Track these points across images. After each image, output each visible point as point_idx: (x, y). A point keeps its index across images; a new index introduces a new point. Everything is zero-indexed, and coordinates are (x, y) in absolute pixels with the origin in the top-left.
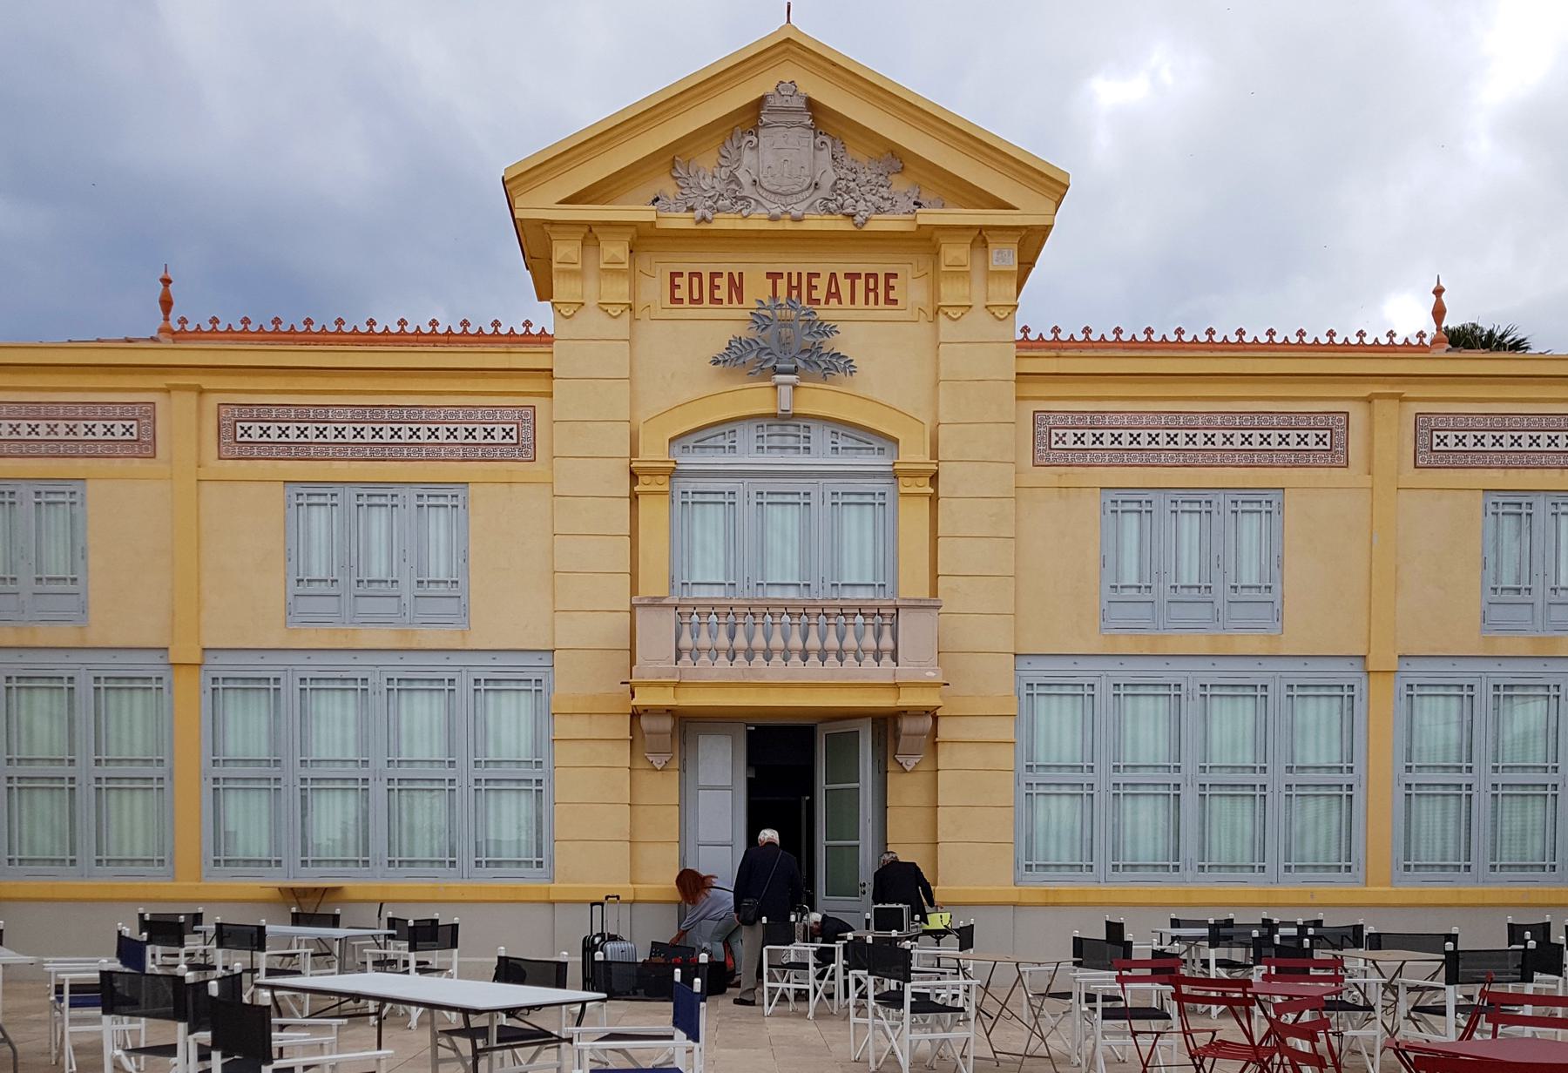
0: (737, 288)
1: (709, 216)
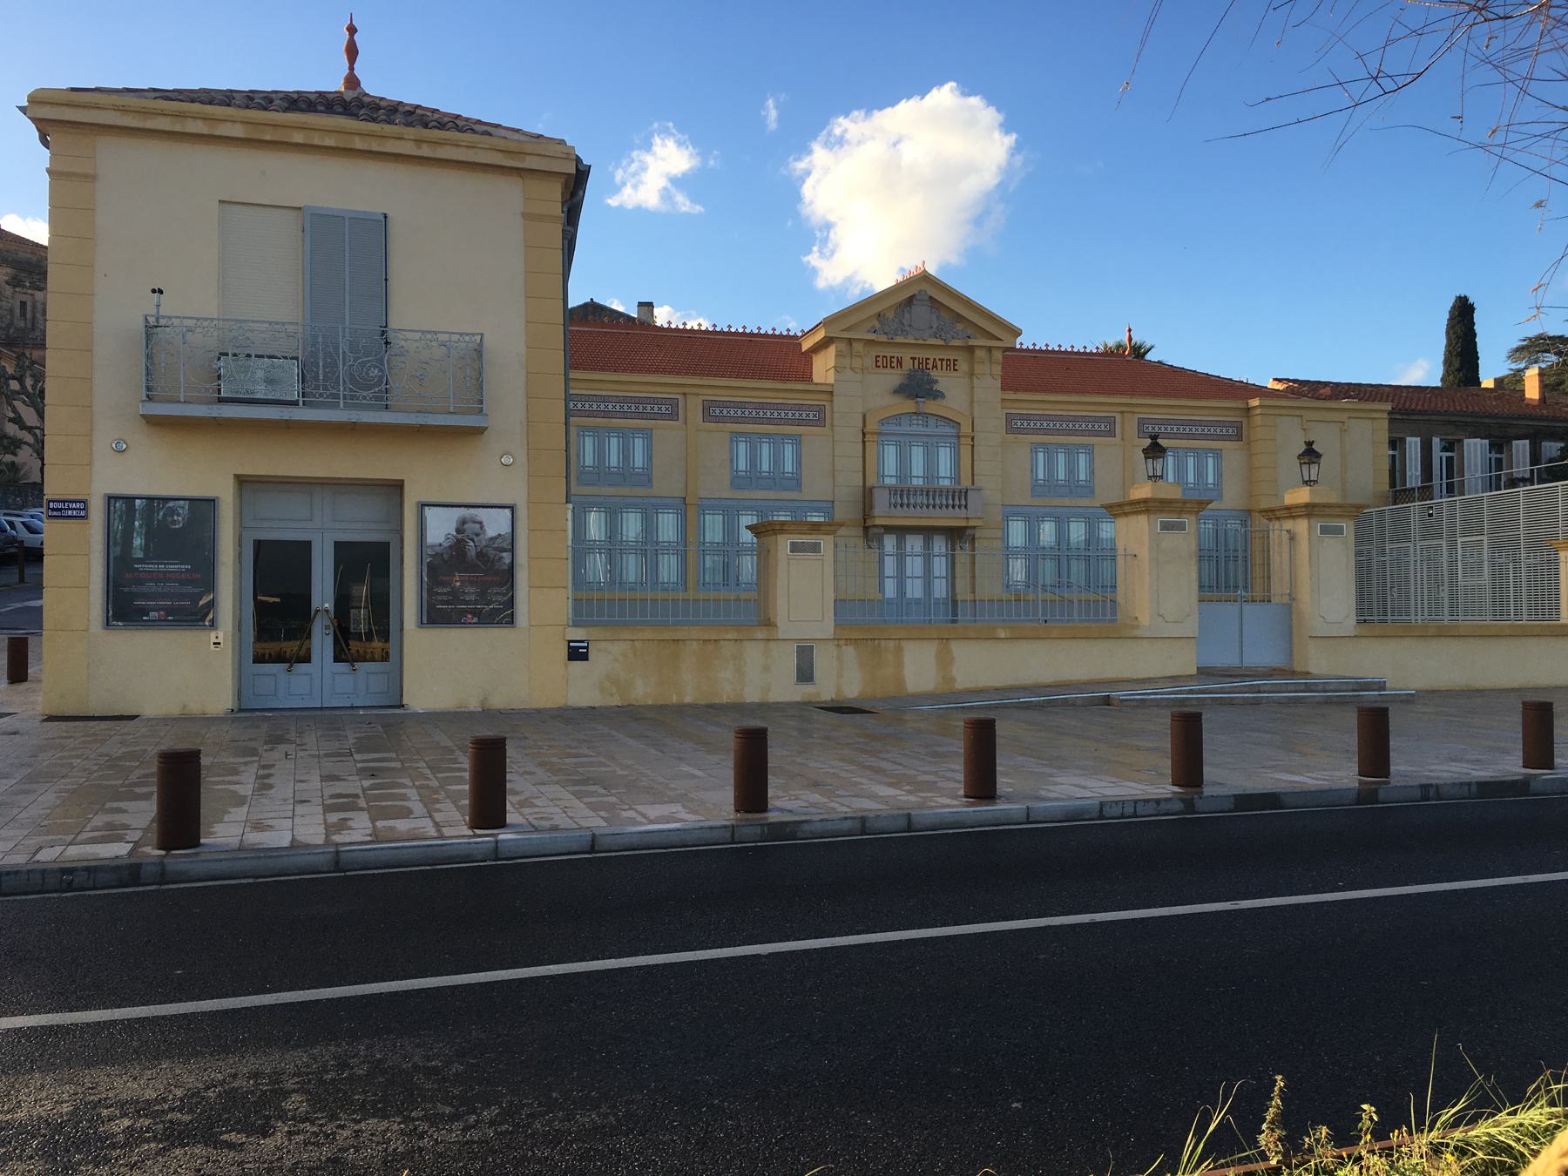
0: (900, 362)
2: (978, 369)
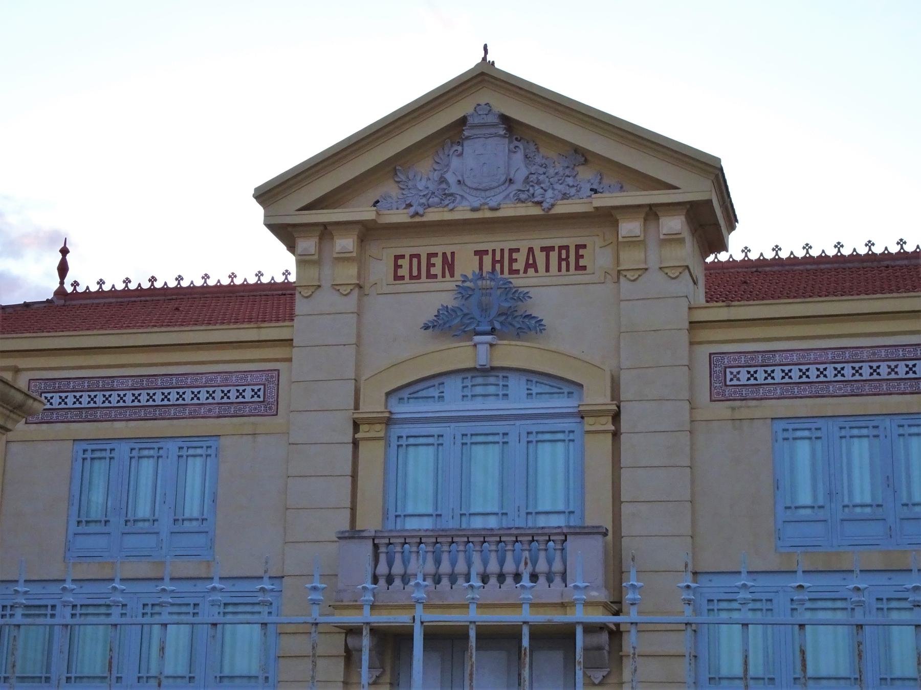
0: (449, 264)
1: (421, 211)
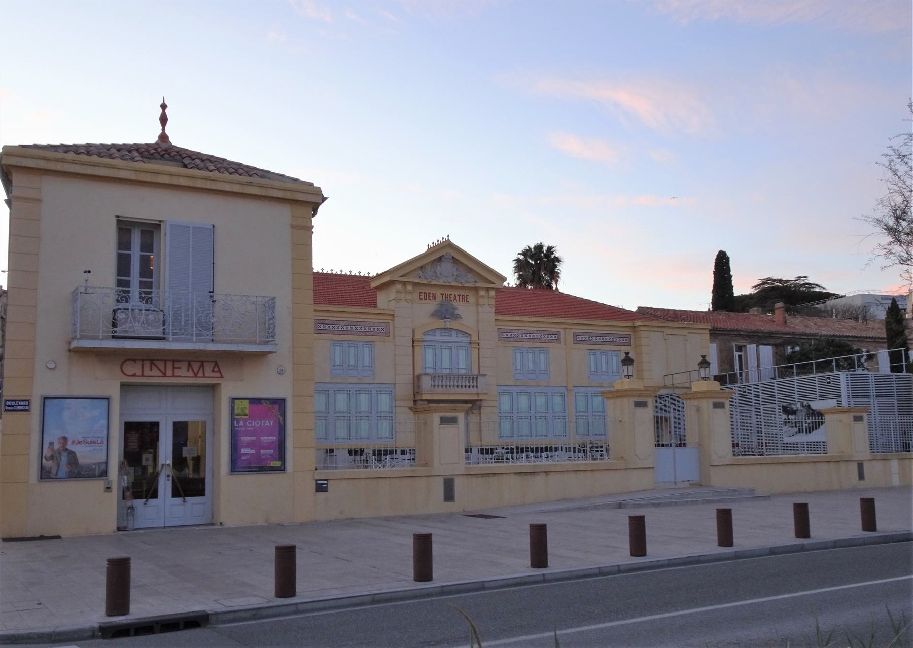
0: (434, 297)
2: (481, 301)
